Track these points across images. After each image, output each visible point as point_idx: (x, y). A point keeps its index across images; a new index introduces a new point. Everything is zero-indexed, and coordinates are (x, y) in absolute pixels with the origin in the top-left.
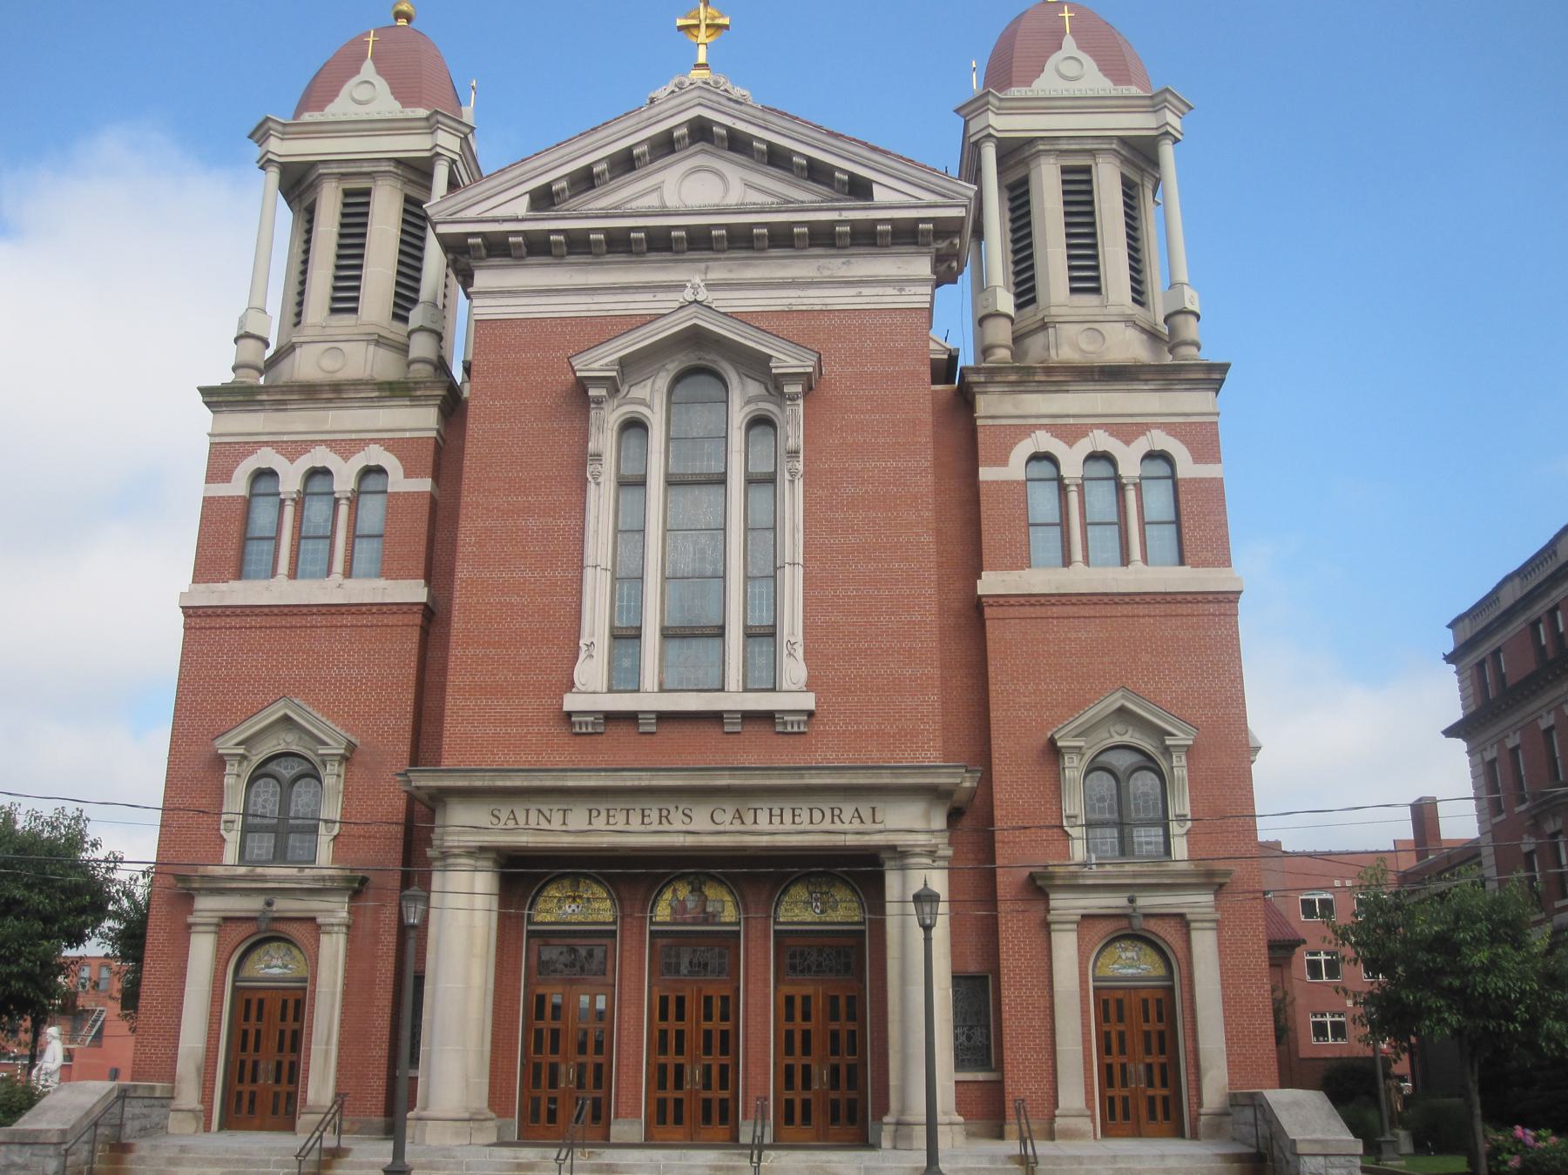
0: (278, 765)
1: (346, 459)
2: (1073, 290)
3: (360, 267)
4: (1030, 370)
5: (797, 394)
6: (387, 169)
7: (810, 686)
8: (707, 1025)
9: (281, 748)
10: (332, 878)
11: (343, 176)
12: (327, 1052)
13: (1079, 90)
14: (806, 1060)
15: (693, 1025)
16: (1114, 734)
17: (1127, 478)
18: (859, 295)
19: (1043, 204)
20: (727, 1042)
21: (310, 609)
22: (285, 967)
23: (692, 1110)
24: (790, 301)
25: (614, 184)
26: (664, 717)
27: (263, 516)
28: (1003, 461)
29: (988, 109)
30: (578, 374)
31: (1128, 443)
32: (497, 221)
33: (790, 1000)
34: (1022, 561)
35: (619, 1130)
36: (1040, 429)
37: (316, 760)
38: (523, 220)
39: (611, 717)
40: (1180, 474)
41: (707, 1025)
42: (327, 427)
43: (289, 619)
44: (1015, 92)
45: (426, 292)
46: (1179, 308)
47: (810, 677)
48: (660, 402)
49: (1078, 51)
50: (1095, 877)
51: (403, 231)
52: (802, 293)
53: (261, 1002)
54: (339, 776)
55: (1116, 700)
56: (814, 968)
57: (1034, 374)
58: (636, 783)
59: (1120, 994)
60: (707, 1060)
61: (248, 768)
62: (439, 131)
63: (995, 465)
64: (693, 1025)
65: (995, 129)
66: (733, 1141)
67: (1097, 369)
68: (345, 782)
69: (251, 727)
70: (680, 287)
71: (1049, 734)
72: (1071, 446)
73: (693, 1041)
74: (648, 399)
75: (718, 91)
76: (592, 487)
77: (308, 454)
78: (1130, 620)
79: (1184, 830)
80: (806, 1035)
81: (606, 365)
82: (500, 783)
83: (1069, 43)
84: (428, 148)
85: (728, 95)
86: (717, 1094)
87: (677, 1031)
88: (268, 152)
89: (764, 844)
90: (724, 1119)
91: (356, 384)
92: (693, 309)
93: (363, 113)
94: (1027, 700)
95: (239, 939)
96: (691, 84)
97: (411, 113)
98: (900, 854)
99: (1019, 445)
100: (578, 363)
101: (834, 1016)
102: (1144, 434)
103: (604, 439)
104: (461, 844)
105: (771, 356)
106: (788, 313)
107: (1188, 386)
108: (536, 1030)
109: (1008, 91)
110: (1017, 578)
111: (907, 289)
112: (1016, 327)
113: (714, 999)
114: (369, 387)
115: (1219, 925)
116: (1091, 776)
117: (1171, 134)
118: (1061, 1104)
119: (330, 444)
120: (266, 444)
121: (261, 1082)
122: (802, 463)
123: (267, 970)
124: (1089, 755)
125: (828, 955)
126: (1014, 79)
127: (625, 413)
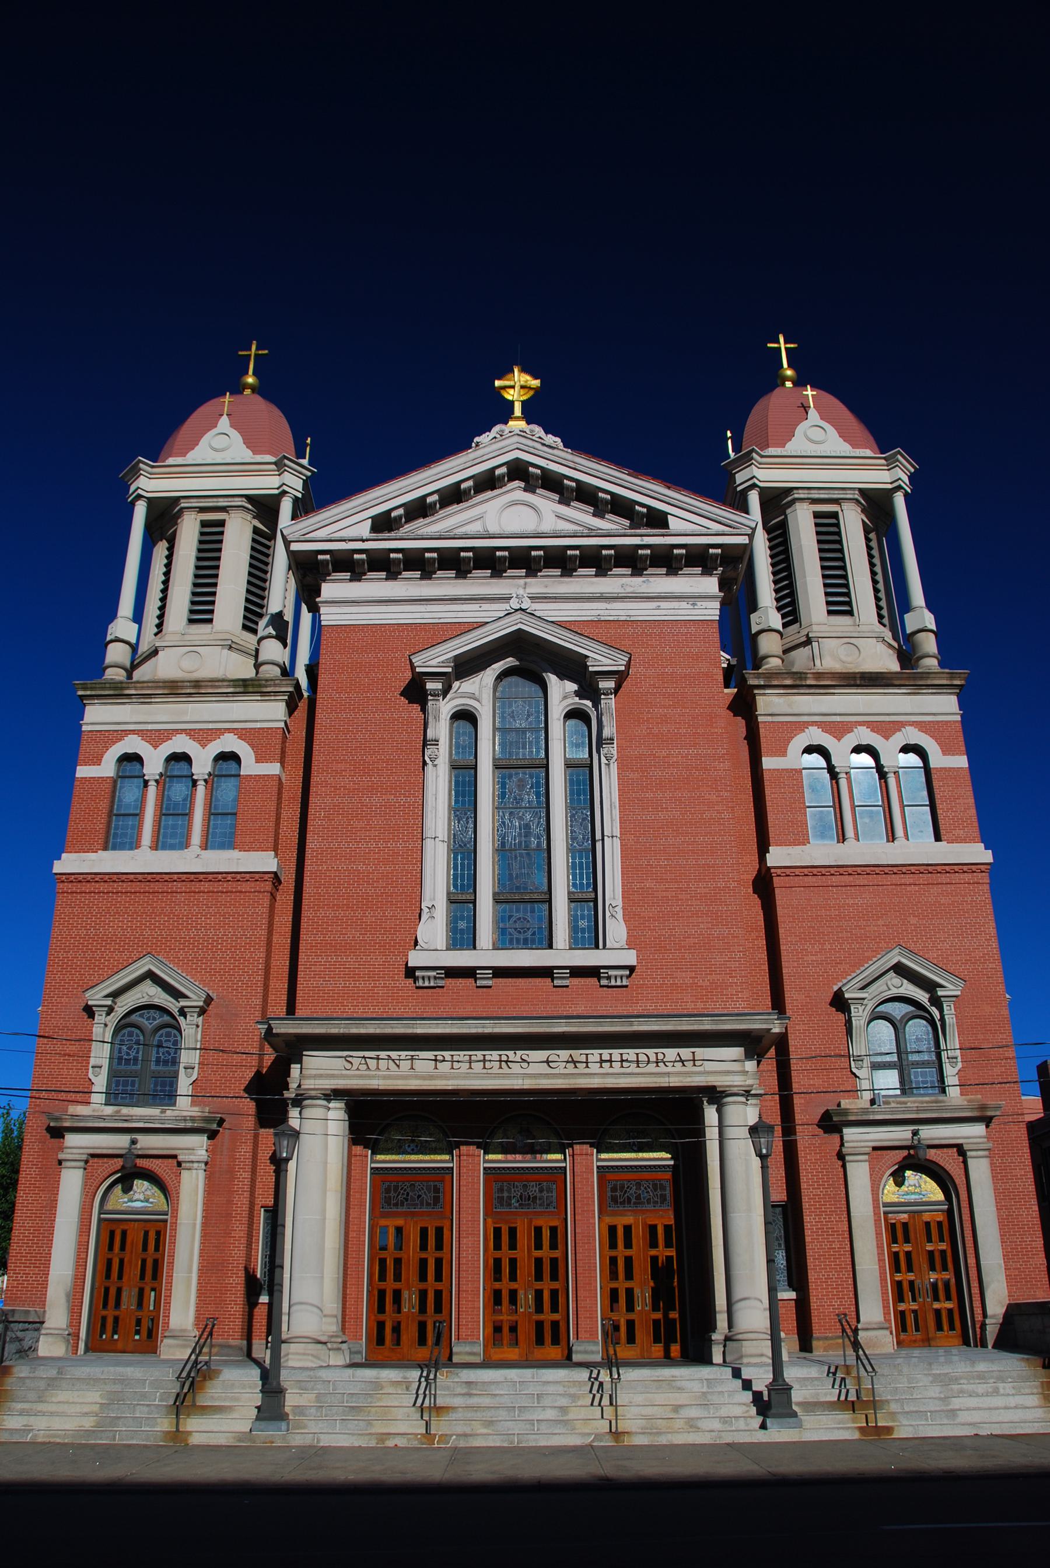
0: (141, 1016)
1: (204, 746)
2: (830, 612)
3: (215, 585)
4: (801, 675)
5: (610, 689)
6: (240, 504)
7: (631, 945)
8: (538, 1253)
9: (145, 1001)
10: (193, 1119)
11: (202, 510)
12: (189, 1279)
13: (824, 451)
14: (629, 1284)
15: (525, 1253)
16: (891, 987)
17: (888, 767)
18: (658, 608)
19: (800, 542)
20: (557, 1269)
21: (171, 876)
22: (147, 1201)
23: (526, 1331)
24: (599, 612)
25: (442, 513)
26: (500, 972)
27: (129, 794)
28: (783, 752)
29: (752, 463)
30: (418, 670)
31: (887, 738)
32: (344, 541)
33: (612, 1230)
34: (802, 840)
35: (461, 1351)
36: (812, 725)
37: (175, 1011)
38: (367, 540)
39: (453, 972)
40: (933, 764)
41: (538, 1253)
42: (188, 719)
43: (152, 885)
44: (771, 451)
45: (274, 606)
46: (921, 627)
47: (629, 936)
48: (487, 696)
49: (822, 421)
50: (885, 1113)
51: (252, 557)
52: (608, 606)
53: (124, 1233)
54: (198, 1026)
55: (895, 957)
56: (633, 1200)
57: (806, 679)
58: (480, 1030)
59: (904, 1217)
60: (538, 1285)
61: (113, 1020)
62: (286, 472)
63: (775, 756)
64: (525, 1253)
65: (758, 479)
66: (567, 1360)
67: (858, 676)
68: (202, 1032)
69: (118, 980)
70: (507, 599)
71: (836, 988)
72: (839, 740)
73: (526, 1269)
74: (477, 694)
75: (534, 438)
76: (429, 768)
77: (170, 741)
78: (899, 888)
79: (956, 1070)
80: (629, 1260)
81: (443, 662)
82: (354, 1031)
83: (813, 413)
84: (277, 486)
85: (542, 441)
86: (548, 1316)
87: (510, 1259)
88: (139, 488)
89: (596, 1086)
90: (556, 1341)
91: (213, 682)
92: (519, 615)
93: (219, 458)
94: (814, 958)
95: (106, 1174)
96: (510, 432)
97: (259, 458)
98: (716, 1095)
99: (798, 736)
100: (417, 660)
101: (654, 1244)
102: (900, 730)
103: (441, 729)
104: (317, 1087)
105: (587, 657)
106: (598, 623)
107: (934, 691)
108: (380, 1259)
109: (766, 451)
110: (801, 852)
111: (699, 603)
112: (785, 641)
113: (544, 1230)
114: (226, 683)
115: (991, 1154)
116: (872, 1024)
117: (903, 488)
118: (862, 1319)
119: (190, 733)
120: (133, 732)
121: (124, 1307)
122: (615, 748)
123: (130, 1204)
124: (870, 1005)
125: (645, 1188)
126: (770, 441)
127: (457, 706)
